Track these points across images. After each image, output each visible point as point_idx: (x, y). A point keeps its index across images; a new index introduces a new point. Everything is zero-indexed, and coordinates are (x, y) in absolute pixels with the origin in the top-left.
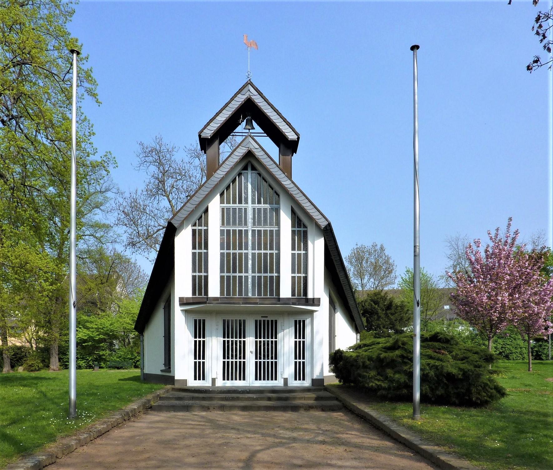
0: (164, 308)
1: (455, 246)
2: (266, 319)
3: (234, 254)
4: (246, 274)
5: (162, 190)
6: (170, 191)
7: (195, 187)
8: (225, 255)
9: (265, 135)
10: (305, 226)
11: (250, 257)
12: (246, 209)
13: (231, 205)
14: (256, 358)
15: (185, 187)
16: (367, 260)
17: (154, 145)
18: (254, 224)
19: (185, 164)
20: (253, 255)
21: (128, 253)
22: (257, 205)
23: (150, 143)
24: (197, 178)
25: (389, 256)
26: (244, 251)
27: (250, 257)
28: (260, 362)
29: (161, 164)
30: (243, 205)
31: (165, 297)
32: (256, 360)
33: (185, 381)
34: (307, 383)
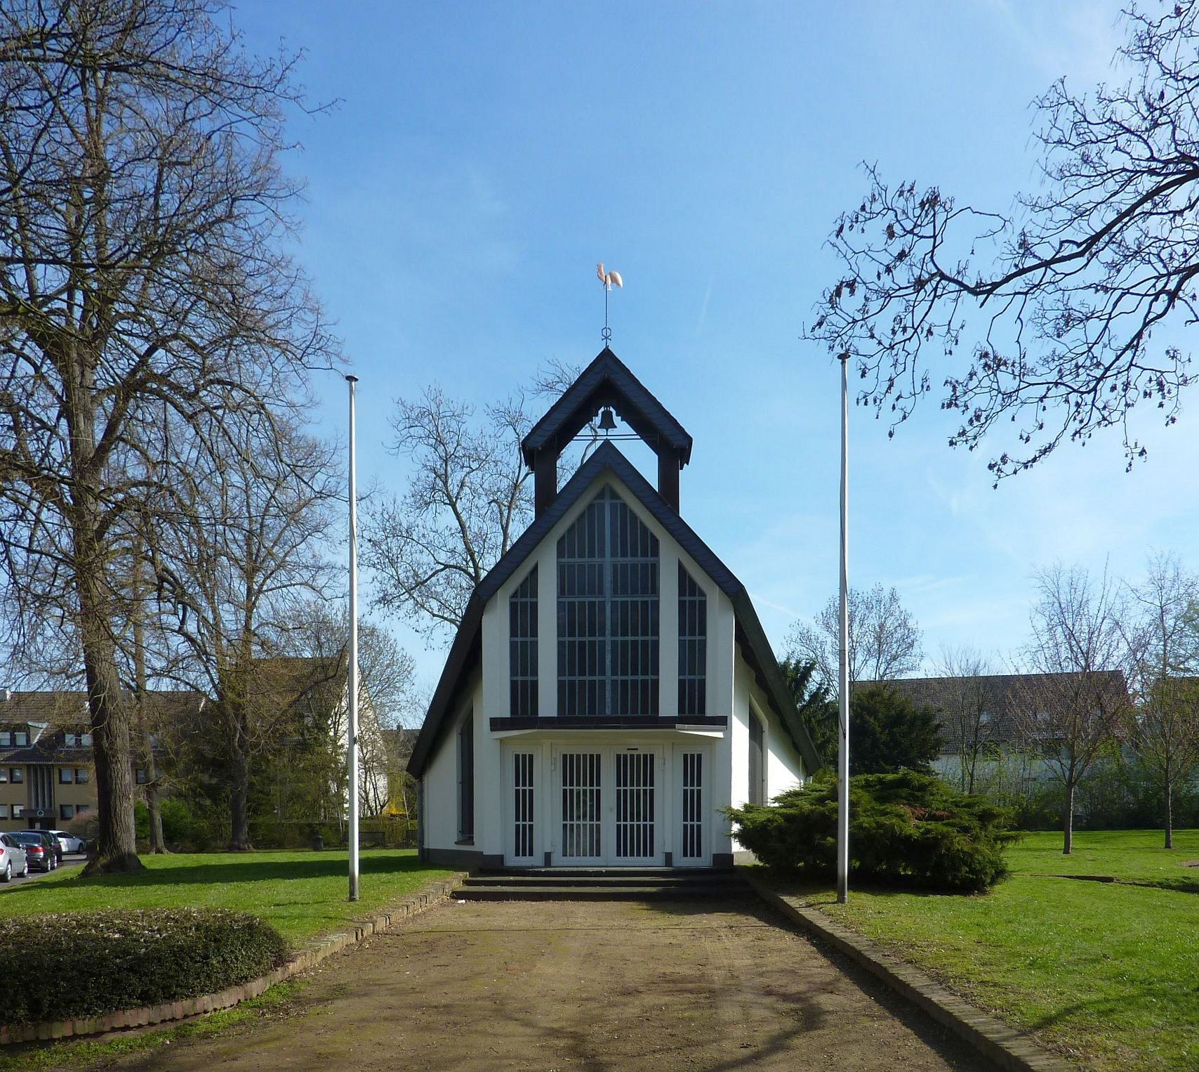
0: (462, 734)
1: (1051, 586)
2: (635, 753)
3: (582, 644)
4: (602, 678)
5: (444, 493)
6: (458, 493)
7: (506, 484)
8: (567, 645)
9: (638, 437)
10: (702, 594)
11: (608, 648)
12: (601, 566)
13: (577, 560)
14: (619, 819)
15: (486, 486)
16: (862, 620)
17: (425, 403)
18: (615, 591)
19: (487, 438)
20: (614, 643)
21: (377, 618)
22: (619, 559)
23: (417, 399)
24: (511, 466)
25: (909, 612)
26: (598, 639)
27: (608, 648)
28: (625, 826)
29: (440, 441)
30: (597, 560)
31: (461, 716)
32: (619, 823)
33: (501, 857)
34: (704, 861)
